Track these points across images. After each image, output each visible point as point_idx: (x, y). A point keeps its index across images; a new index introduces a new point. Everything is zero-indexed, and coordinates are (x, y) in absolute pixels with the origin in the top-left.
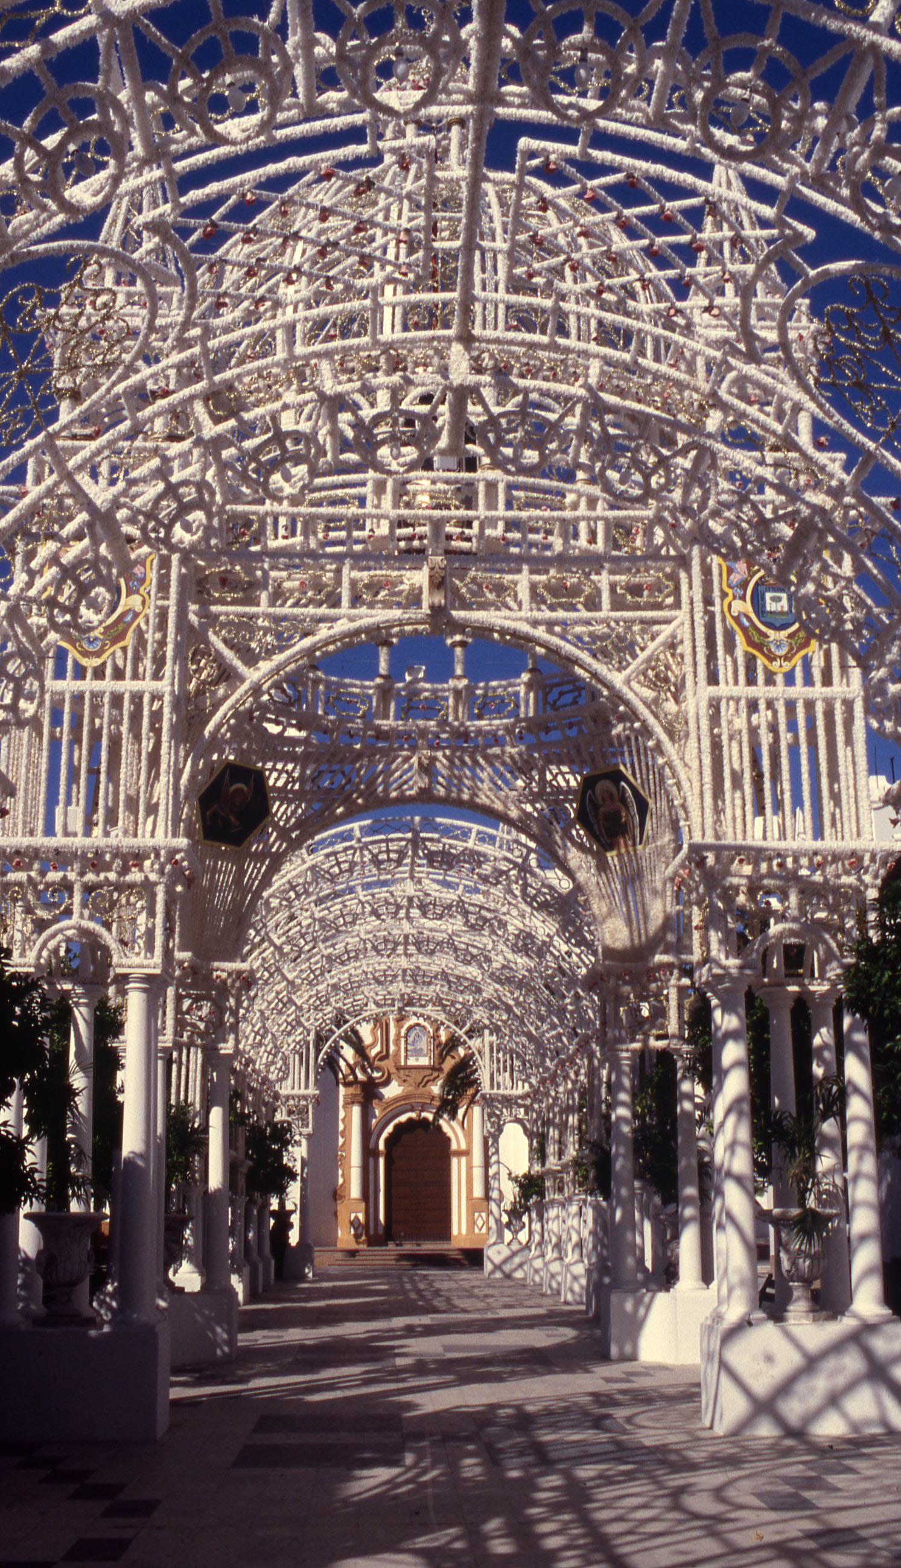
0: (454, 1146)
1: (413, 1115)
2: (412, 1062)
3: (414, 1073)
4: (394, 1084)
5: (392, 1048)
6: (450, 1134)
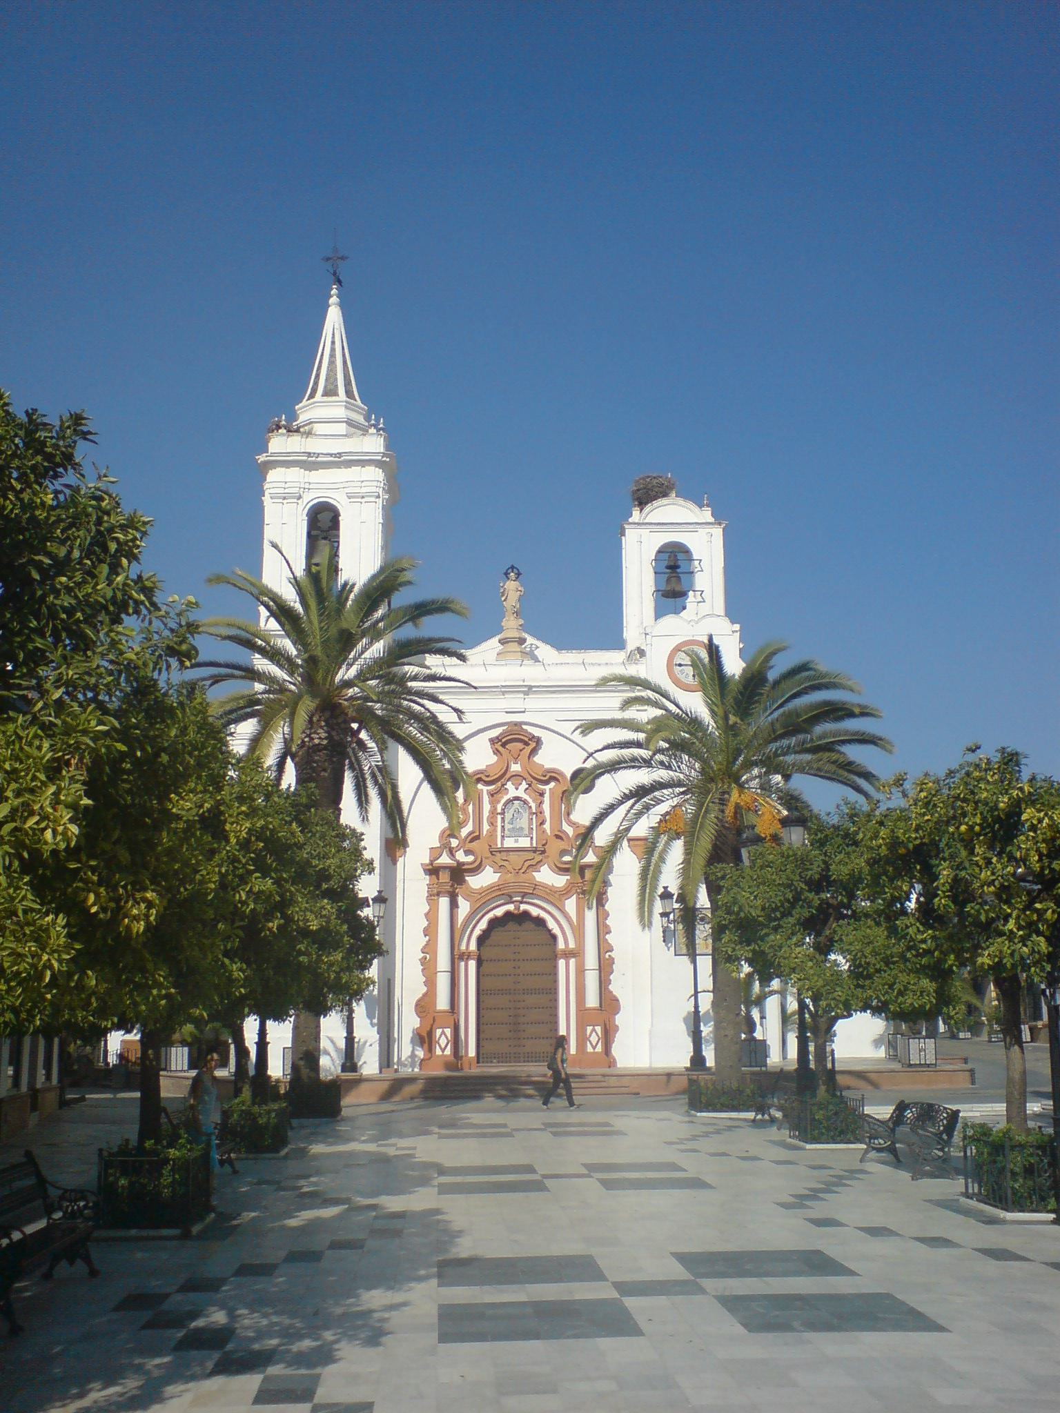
0: (561, 945)
1: (511, 907)
2: (509, 843)
3: (512, 857)
4: (488, 870)
5: (486, 827)
6: (556, 930)
